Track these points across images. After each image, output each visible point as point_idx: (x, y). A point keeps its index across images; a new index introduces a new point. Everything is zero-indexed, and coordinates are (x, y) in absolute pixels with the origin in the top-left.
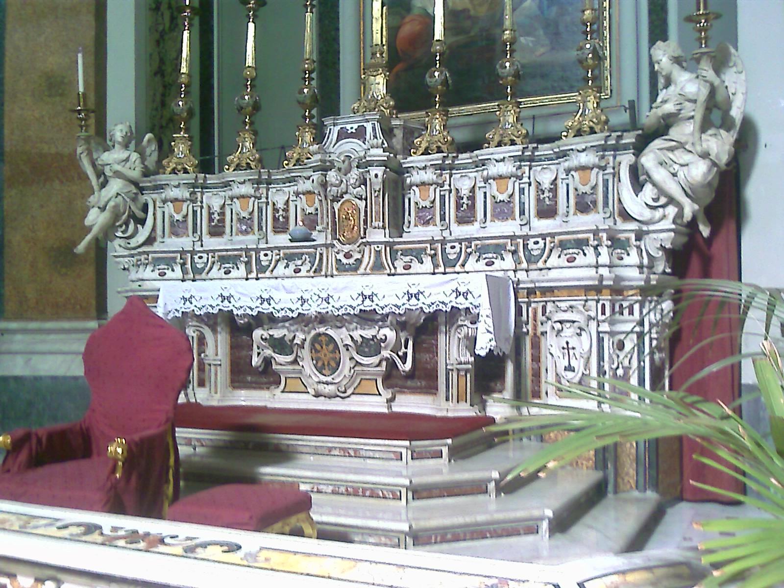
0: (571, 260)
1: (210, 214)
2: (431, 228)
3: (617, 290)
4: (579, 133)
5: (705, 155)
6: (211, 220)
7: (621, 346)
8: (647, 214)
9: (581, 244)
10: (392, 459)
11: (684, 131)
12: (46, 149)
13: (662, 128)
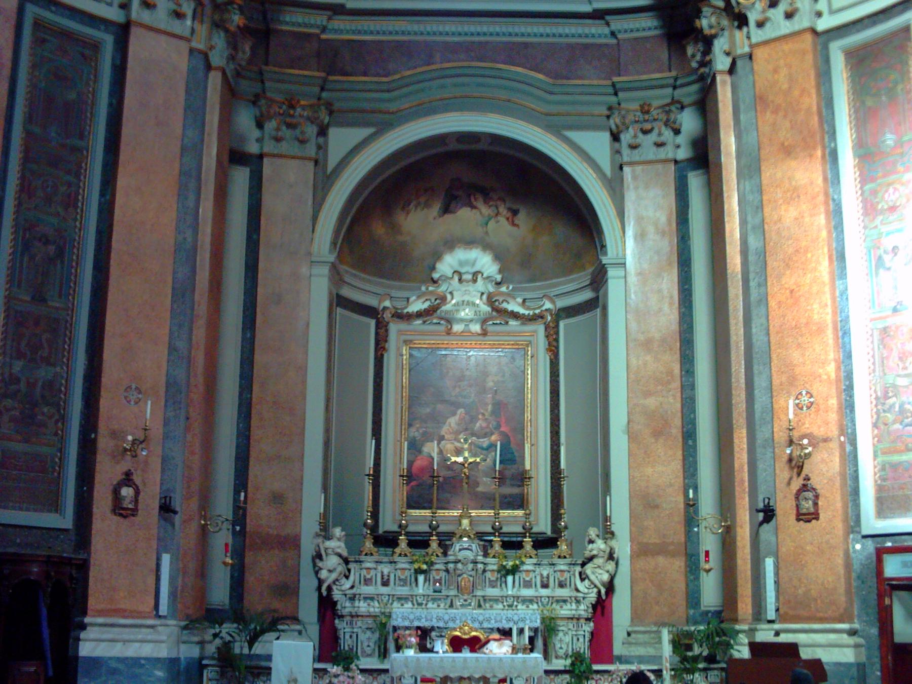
0: (528, 607)
1: (382, 576)
2: (495, 589)
4: (559, 557)
5: (608, 572)
6: (382, 578)
7: (578, 639)
8: (586, 591)
11: (598, 561)
12: (271, 532)
13: (591, 559)
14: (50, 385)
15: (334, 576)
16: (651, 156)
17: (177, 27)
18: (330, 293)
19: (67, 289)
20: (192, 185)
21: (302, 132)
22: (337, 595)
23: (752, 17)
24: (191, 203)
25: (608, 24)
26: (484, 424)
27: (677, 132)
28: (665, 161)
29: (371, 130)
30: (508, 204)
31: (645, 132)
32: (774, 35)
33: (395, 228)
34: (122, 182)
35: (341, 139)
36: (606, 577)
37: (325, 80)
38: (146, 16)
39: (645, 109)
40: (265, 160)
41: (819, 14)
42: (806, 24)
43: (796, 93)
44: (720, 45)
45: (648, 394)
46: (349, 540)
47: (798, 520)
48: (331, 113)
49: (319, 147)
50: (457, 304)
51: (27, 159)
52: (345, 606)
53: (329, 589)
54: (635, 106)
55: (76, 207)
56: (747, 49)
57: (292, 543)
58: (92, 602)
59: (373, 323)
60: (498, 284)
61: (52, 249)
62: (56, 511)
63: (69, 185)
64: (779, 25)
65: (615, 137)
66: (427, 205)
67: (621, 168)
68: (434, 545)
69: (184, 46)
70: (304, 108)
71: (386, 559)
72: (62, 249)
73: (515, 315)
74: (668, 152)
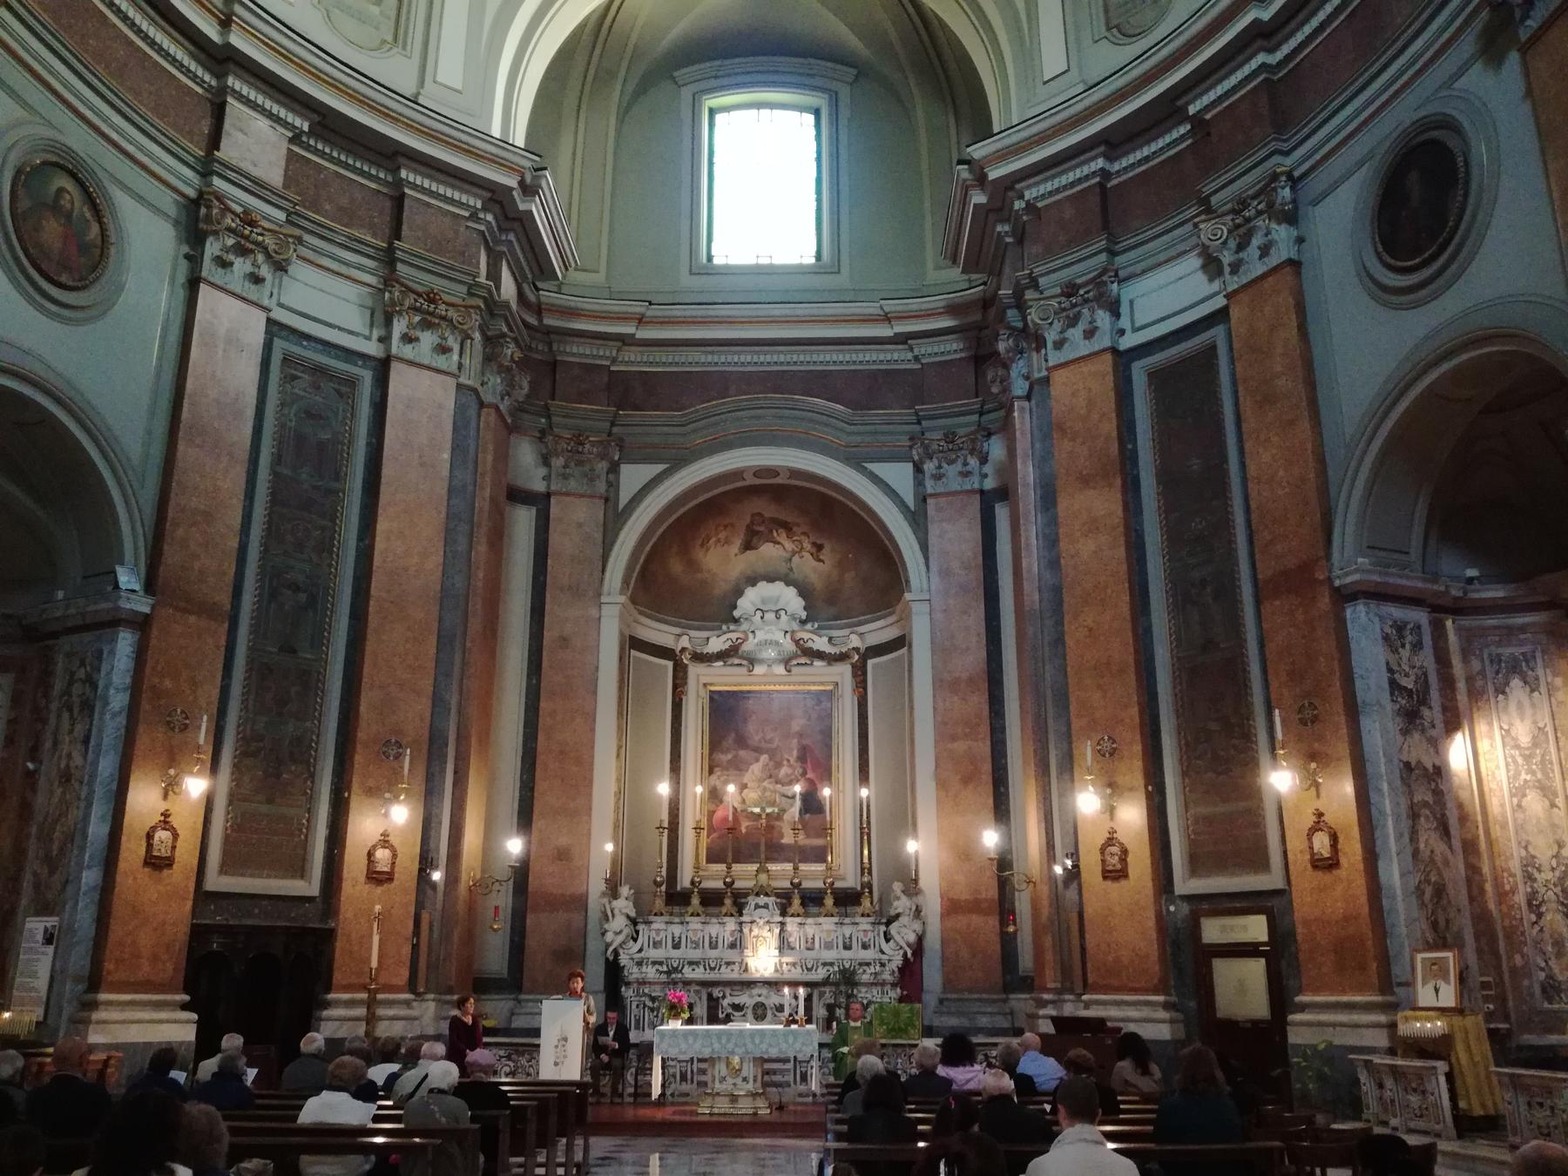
3: (883, 984)
9: (868, 964)
10: (158, 211)
11: (904, 920)
15: (620, 938)
16: (955, 487)
17: (441, 362)
18: (622, 634)
19: (319, 641)
20: (464, 528)
21: (592, 470)
22: (624, 960)
23: (1051, 336)
24: (462, 546)
25: (911, 349)
26: (789, 771)
27: (984, 460)
28: (972, 491)
29: (660, 467)
30: (813, 539)
31: (951, 462)
32: (1071, 357)
33: (692, 565)
34: (382, 526)
35: (633, 476)
36: (912, 938)
37: (616, 415)
39: (950, 437)
40: (553, 500)
41: (1122, 332)
42: (1107, 343)
43: (1096, 416)
45: (954, 738)
46: (637, 900)
47: (1105, 878)
48: (621, 449)
49: (610, 484)
50: (759, 644)
51: (275, 499)
52: (632, 973)
53: (616, 953)
54: (938, 435)
55: (331, 552)
56: (1044, 373)
57: (580, 902)
58: (338, 977)
59: (670, 664)
60: (803, 622)
61: (303, 597)
62: (302, 877)
63: (323, 529)
64: (1078, 344)
65: (918, 469)
66: (727, 542)
67: (924, 500)
68: (728, 902)
69: (451, 382)
70: (593, 444)
71: (677, 920)
72: (316, 599)
73: (820, 655)
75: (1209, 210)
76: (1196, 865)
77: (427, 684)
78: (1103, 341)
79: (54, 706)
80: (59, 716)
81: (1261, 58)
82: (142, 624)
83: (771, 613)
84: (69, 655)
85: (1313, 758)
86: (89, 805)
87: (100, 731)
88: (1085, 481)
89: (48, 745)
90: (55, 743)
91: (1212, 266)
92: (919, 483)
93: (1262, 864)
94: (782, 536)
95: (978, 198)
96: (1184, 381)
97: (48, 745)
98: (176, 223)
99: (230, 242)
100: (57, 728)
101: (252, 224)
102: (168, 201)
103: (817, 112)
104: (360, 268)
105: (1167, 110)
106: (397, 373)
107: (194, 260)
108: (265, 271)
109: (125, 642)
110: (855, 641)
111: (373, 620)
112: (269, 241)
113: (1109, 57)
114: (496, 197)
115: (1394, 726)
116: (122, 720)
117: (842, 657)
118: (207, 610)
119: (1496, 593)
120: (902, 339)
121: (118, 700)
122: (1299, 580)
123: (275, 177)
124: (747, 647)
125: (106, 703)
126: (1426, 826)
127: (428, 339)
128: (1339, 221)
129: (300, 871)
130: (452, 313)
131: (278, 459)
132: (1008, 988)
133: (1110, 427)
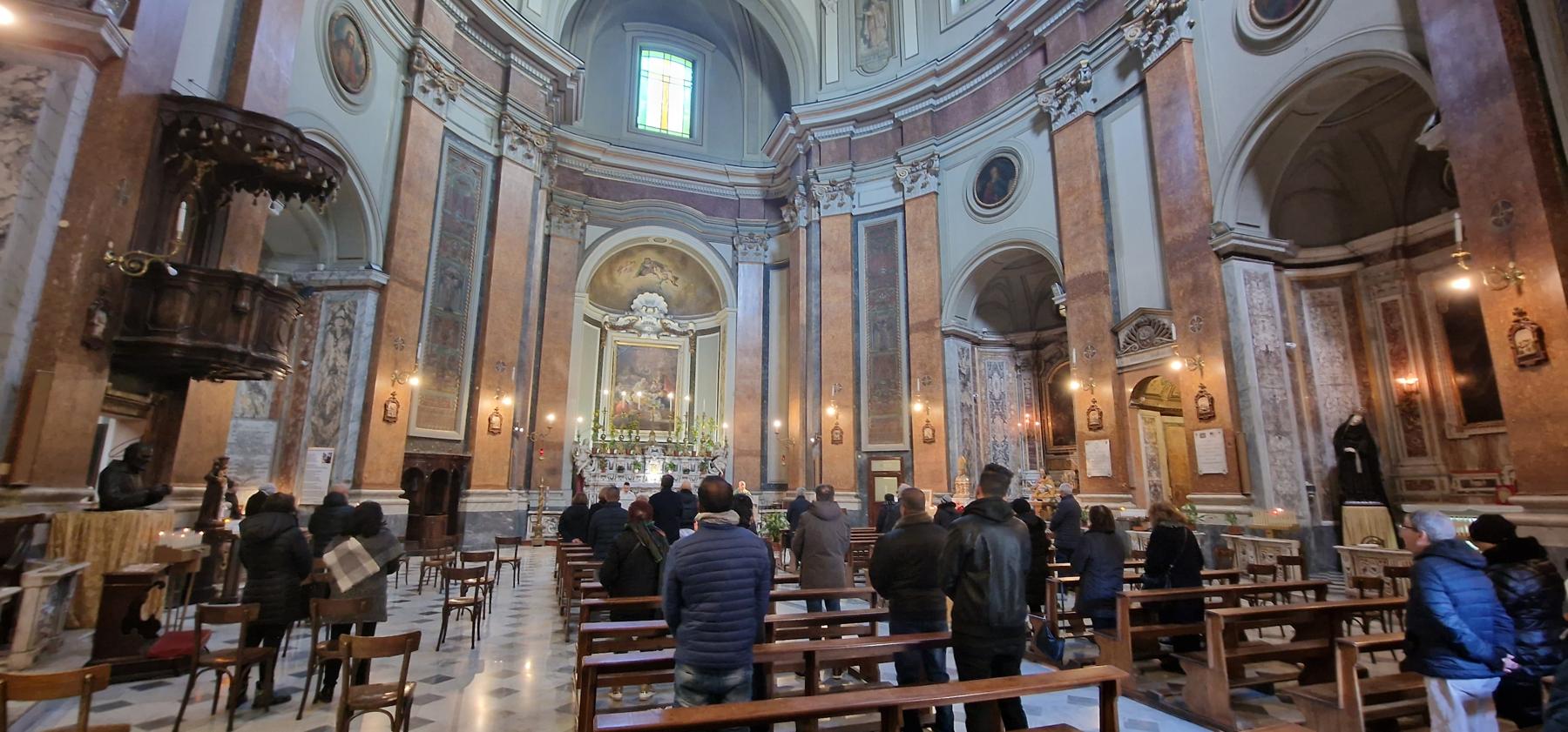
14: (453, 359)
19: (464, 305)
22: (585, 475)
33: (612, 280)
34: (497, 247)
38: (511, 154)
39: (751, 236)
44: (803, 213)
51: (443, 228)
58: (474, 482)
64: (834, 209)
72: (462, 284)
73: (673, 332)
74: (762, 259)
75: (899, 161)
76: (872, 439)
77: (517, 334)
78: (846, 209)
79: (321, 330)
80: (325, 337)
81: (932, 101)
82: (381, 289)
83: (650, 310)
84: (329, 302)
85: (929, 399)
86: (352, 388)
87: (357, 348)
88: (835, 270)
89: (317, 351)
90: (323, 352)
91: (898, 185)
92: (735, 256)
93: (900, 439)
94: (657, 270)
95: (792, 130)
96: (883, 236)
97: (317, 351)
98: (398, 62)
99: (427, 78)
100: (324, 344)
101: (439, 70)
102: (396, 49)
103: (694, 63)
104: (487, 104)
105: (886, 113)
106: (505, 162)
107: (408, 86)
108: (444, 98)
109: (371, 298)
110: (691, 326)
111: (492, 297)
112: (446, 81)
113: (858, 81)
114: (558, 78)
115: (959, 388)
116: (370, 342)
117: (685, 334)
118: (414, 285)
119: (993, 338)
120: (733, 185)
121: (368, 331)
122: (928, 326)
123: (449, 44)
124: (638, 324)
125: (361, 332)
126: (967, 427)
127: (521, 149)
128: (959, 178)
129: (901, 440)
130: (533, 137)
131: (445, 205)
132: (763, 489)
133: (848, 248)
